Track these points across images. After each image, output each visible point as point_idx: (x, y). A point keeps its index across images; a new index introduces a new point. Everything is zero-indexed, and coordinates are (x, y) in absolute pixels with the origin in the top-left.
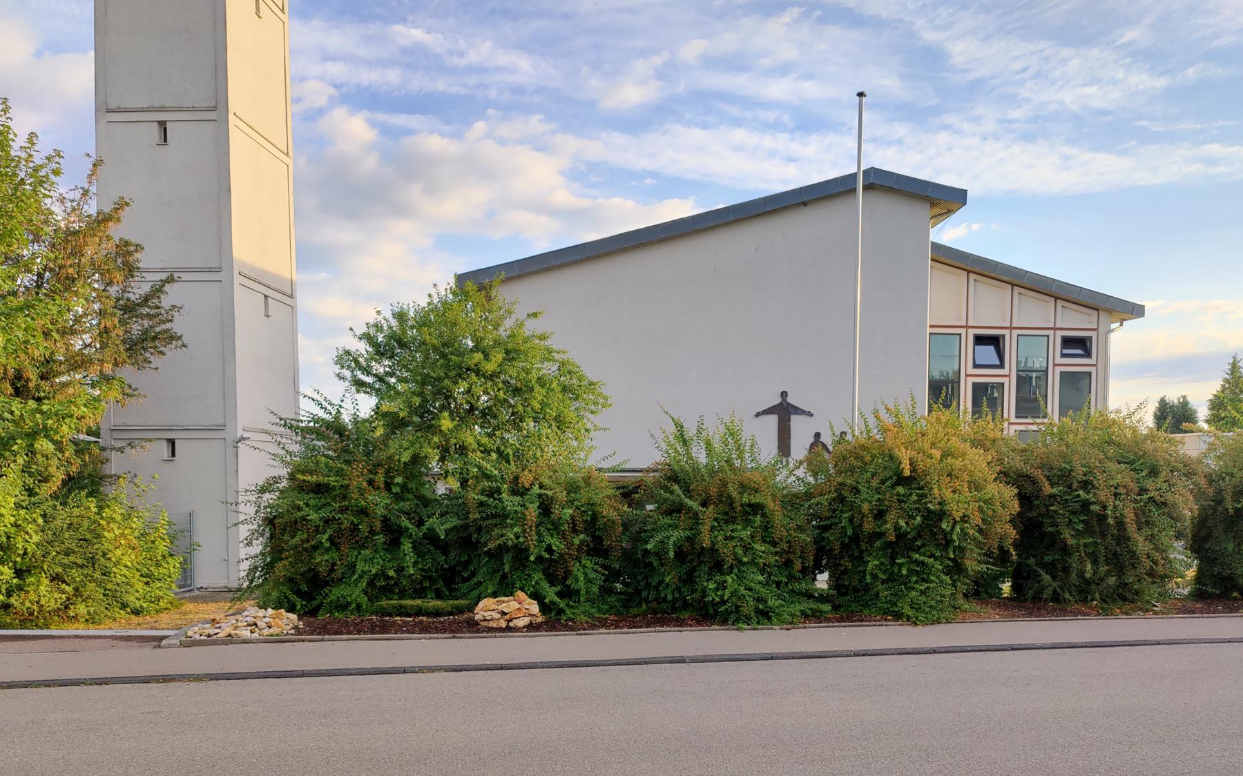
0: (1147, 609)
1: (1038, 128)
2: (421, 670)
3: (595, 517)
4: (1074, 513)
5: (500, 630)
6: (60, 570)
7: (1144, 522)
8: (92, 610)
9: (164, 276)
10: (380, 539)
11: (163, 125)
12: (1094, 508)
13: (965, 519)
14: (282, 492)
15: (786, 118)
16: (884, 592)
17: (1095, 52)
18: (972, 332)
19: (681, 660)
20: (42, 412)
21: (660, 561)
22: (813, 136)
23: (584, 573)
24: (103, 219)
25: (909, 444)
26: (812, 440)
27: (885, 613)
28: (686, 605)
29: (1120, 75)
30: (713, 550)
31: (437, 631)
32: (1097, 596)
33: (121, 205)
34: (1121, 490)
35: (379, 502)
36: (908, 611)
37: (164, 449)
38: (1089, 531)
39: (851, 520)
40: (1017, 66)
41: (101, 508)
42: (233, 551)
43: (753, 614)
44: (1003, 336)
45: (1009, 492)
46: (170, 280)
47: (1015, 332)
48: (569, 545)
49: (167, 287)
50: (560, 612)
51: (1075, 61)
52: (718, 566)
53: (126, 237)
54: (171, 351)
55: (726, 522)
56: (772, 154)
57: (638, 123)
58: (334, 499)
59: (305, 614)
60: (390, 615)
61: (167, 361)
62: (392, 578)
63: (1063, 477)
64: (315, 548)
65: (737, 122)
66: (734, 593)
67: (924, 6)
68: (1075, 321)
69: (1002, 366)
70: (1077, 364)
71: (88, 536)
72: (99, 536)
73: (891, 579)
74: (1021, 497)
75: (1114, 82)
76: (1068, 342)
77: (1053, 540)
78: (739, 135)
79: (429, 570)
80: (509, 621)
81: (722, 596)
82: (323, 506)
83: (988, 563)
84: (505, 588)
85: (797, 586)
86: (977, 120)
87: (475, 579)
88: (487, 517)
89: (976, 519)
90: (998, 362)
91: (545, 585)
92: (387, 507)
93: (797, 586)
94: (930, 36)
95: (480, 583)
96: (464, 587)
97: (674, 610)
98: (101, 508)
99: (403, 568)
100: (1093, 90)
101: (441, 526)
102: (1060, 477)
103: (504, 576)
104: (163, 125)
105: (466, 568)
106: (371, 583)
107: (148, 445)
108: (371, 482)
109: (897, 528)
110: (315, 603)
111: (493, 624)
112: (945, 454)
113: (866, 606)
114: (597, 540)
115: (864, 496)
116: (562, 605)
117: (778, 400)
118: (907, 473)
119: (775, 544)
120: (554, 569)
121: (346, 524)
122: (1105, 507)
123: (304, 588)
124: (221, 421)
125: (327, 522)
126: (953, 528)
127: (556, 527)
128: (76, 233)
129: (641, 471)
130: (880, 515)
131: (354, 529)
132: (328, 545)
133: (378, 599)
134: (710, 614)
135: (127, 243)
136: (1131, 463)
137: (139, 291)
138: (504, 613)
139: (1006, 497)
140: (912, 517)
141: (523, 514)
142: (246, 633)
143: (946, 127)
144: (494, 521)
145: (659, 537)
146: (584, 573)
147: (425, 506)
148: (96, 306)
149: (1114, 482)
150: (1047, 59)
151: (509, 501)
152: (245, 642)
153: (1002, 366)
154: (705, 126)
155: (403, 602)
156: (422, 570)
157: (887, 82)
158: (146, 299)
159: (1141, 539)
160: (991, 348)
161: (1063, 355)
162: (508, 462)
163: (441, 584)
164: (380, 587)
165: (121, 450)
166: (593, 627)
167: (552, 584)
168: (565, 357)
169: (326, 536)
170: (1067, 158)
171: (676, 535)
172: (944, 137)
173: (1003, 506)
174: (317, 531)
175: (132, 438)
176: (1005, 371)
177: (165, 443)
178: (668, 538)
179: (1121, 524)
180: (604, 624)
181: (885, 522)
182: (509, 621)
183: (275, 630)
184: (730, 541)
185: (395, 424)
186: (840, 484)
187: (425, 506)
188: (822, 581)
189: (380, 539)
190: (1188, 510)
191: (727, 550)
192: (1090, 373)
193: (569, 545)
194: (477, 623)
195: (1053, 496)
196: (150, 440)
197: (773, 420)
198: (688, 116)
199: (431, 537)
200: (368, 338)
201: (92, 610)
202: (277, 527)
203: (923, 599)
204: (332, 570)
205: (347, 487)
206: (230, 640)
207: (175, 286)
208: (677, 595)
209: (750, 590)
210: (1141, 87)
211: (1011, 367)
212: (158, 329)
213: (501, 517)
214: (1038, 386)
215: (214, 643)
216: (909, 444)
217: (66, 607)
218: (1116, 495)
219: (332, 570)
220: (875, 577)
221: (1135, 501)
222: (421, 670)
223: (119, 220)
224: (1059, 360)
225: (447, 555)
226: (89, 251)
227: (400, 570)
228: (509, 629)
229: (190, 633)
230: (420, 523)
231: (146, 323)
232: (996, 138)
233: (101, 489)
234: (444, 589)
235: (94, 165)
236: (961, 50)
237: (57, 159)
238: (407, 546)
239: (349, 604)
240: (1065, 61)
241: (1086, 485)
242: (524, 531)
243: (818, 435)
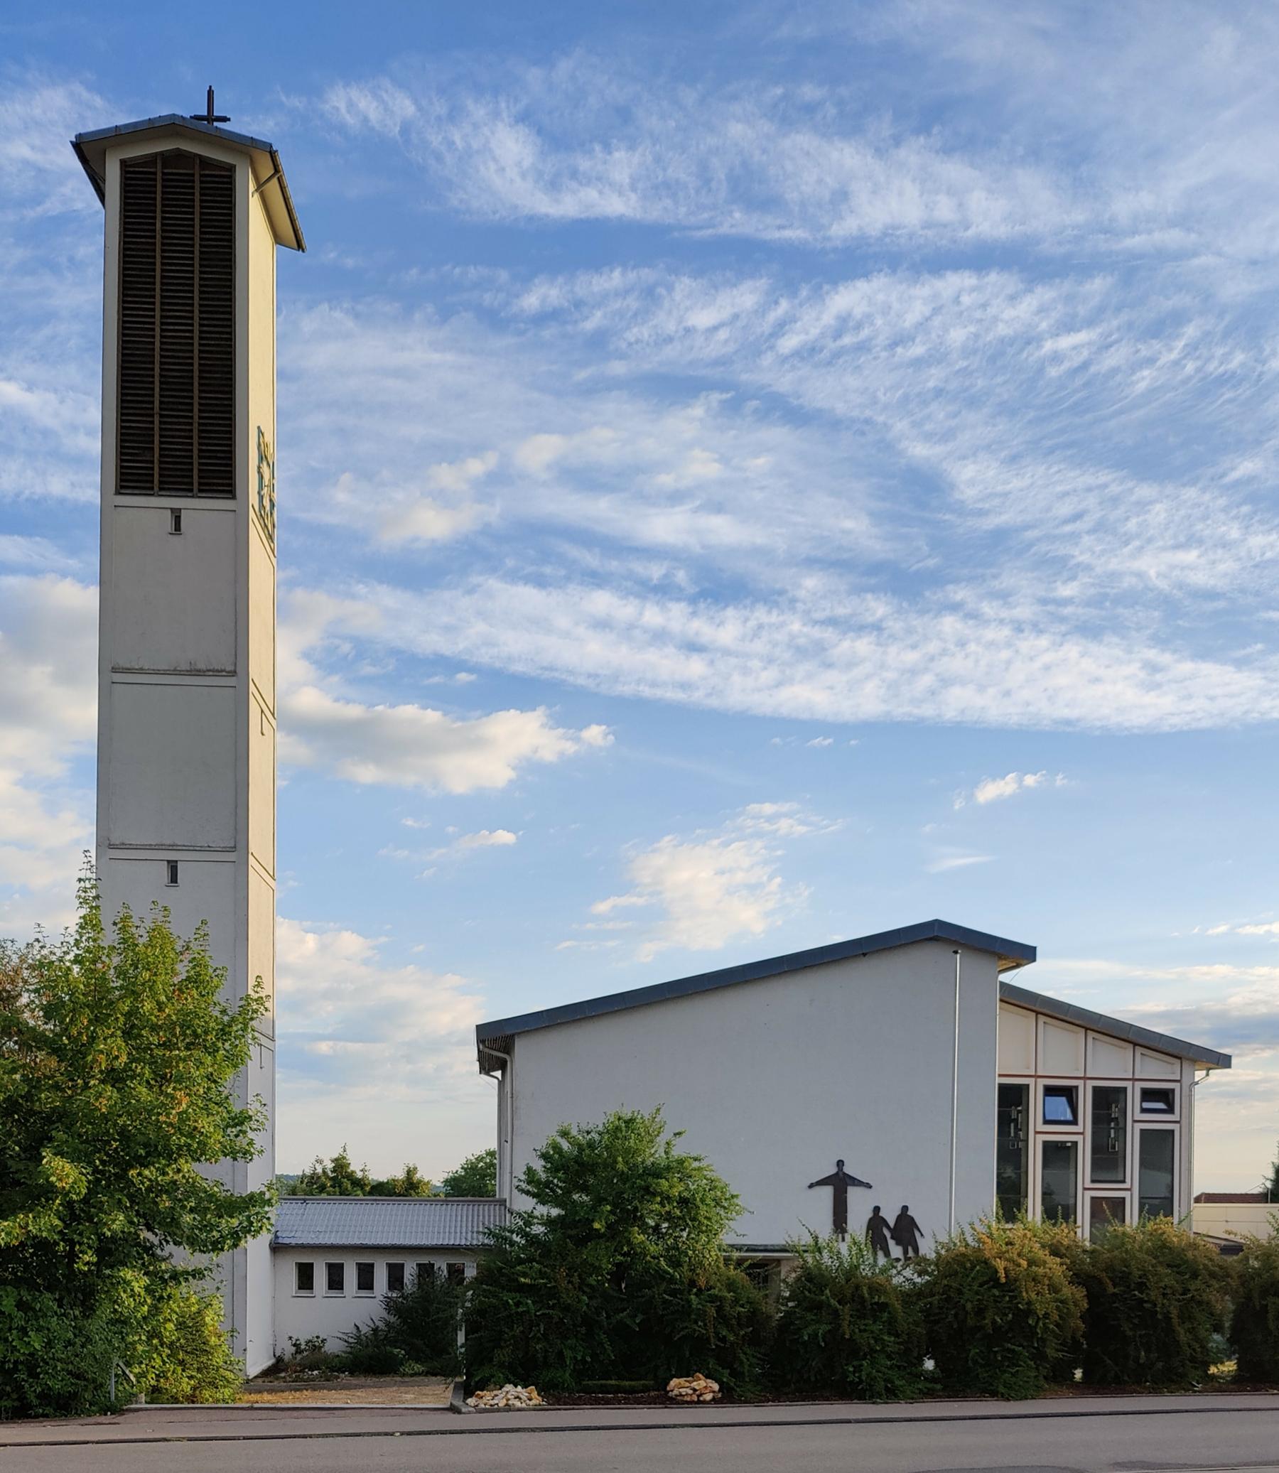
0: (1188, 1389)
1: (1106, 616)
5: (692, 1402)
7: (1186, 1316)
11: (173, 867)
12: (1147, 1305)
13: (1046, 1316)
15: (681, 576)
17: (1190, 493)
19: (849, 1422)
22: (730, 612)
25: (1000, 1255)
26: (871, 1215)
29: (1235, 533)
32: (1149, 1377)
34: (1168, 1291)
39: (956, 1315)
40: (1065, 509)
45: (1080, 1293)
51: (1158, 507)
56: (659, 637)
57: (419, 572)
63: (1122, 1278)
65: (597, 579)
67: (906, 399)
68: (1156, 1071)
69: (1074, 1122)
74: (1089, 1296)
75: (1225, 544)
76: (1148, 1095)
78: (602, 601)
80: (699, 1396)
81: (859, 1377)
86: (1004, 597)
89: (1055, 1316)
90: (1069, 1117)
94: (919, 451)
100: (1191, 556)
102: (1121, 1278)
104: (173, 867)
112: (1031, 1263)
115: (966, 1297)
117: (833, 1170)
118: (1003, 1280)
119: (897, 1336)
121: (556, 1319)
122: (1155, 1305)
126: (1037, 1323)
130: (980, 1312)
136: (1178, 1266)
138: (695, 1390)
140: (1007, 1315)
143: (955, 608)
145: (810, 1330)
149: (1162, 1284)
150: (1115, 500)
152: (519, 1410)
153: (1074, 1122)
154: (540, 582)
157: (849, 524)
159: (1182, 1331)
161: (1144, 1111)
170: (1153, 668)
172: (950, 624)
173: (1076, 1305)
179: (1167, 1317)
181: (984, 1318)
190: (1225, 1305)
192: (1173, 1131)
195: (1114, 1294)
197: (827, 1192)
198: (510, 563)
200: (545, 1156)
203: (1014, 1379)
210: (1269, 555)
214: (1116, 1139)
215: (499, 1410)
216: (1000, 1255)
218: (1164, 1294)
221: (1179, 1300)
228: (699, 1402)
232: (1038, 629)
236: (972, 478)
240: (1143, 506)
241: (1142, 1286)
243: (877, 1209)
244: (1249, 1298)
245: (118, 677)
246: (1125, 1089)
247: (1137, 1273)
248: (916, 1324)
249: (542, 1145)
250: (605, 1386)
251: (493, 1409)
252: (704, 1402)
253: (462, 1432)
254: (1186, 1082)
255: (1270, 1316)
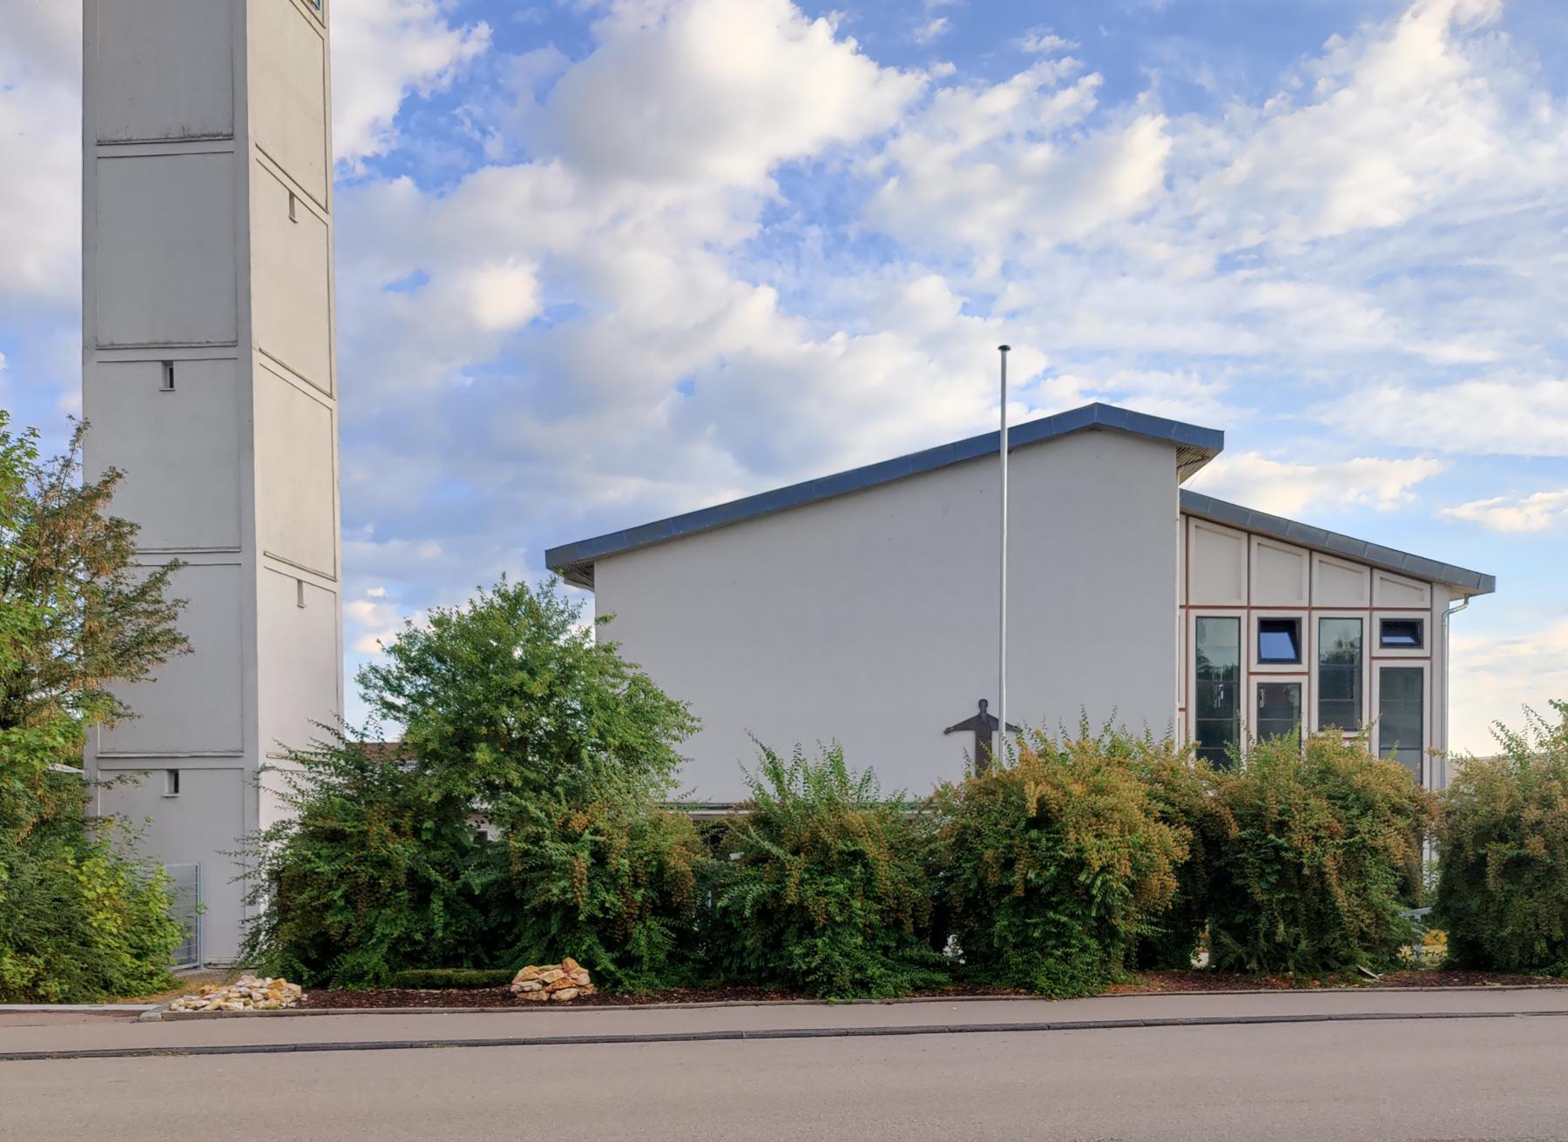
2: (430, 1045)
3: (662, 867)
4: (1265, 861)
5: (540, 1003)
6: (27, 937)
8: (66, 987)
9: (166, 560)
10: (404, 895)
11: (168, 365)
12: (1290, 855)
14: (292, 840)
16: (1015, 958)
18: (1255, 615)
20: (9, 743)
21: (753, 924)
23: (648, 936)
24: (91, 496)
27: (1018, 985)
28: (773, 976)
30: (801, 907)
31: (465, 1003)
32: (1291, 964)
33: (113, 476)
34: (1322, 833)
35: (403, 852)
36: (1042, 982)
37: (165, 781)
38: (1283, 883)
41: (80, 860)
42: (231, 910)
43: (848, 985)
44: (1299, 620)
46: (174, 566)
47: (1316, 615)
48: (629, 902)
49: (170, 577)
50: (618, 983)
52: (808, 928)
53: (118, 516)
54: (173, 657)
55: (822, 874)
58: (351, 848)
59: (315, 986)
60: (414, 987)
61: (169, 670)
62: (419, 942)
63: (1253, 816)
64: (327, 907)
66: (825, 960)
68: (1400, 599)
69: (1298, 660)
70: (1402, 657)
71: (65, 896)
72: (77, 896)
73: (1024, 943)
76: (1389, 627)
77: (1241, 897)
79: (465, 933)
82: (337, 857)
83: (1151, 923)
84: (552, 955)
85: (908, 952)
87: (519, 945)
88: (532, 869)
89: (1124, 868)
90: (1291, 654)
91: (600, 951)
92: (413, 858)
93: (908, 952)
95: (525, 949)
96: (506, 955)
97: (760, 982)
98: (80, 860)
99: (433, 931)
101: (477, 881)
103: (553, 941)
104: (168, 365)
105: (509, 932)
106: (393, 949)
107: (142, 778)
108: (396, 828)
109: (1027, 882)
110: (326, 973)
111: (531, 996)
113: (998, 976)
114: (664, 896)
116: (619, 975)
117: (975, 712)
119: (879, 900)
120: (611, 931)
121: (363, 878)
123: (313, 955)
124: (238, 746)
125: (342, 875)
127: (613, 880)
128: (55, 514)
129: (727, 807)
130: (1008, 865)
131: (373, 883)
132: (342, 903)
133: (402, 968)
134: (797, 986)
135: (119, 523)
136: (1344, 798)
137: (134, 582)
138: (545, 984)
139: (1173, 843)
141: (571, 864)
142: (238, 1005)
144: (542, 873)
145: (736, 891)
146: (648, 936)
147: (463, 856)
148: (80, 603)
151: (555, 850)
152: (237, 1015)
153: (1298, 660)
155: (432, 972)
156: (456, 933)
158: (143, 592)
160: (1285, 636)
161: (1384, 645)
162: (559, 802)
163: (479, 951)
164: (405, 953)
165: (108, 785)
166: (654, 1000)
167: (609, 949)
168: (638, 672)
169: (339, 893)
171: (756, 890)
174: (330, 887)
175: (127, 768)
176: (1303, 668)
177: (166, 774)
178: (747, 892)
180: (667, 997)
182: (552, 992)
183: (272, 1002)
184: (822, 897)
185: (428, 757)
186: (964, 827)
187: (463, 856)
188: (951, 948)
189: (404, 895)
191: (819, 908)
193: (629, 902)
194: (513, 996)
195: (1243, 841)
196: (146, 772)
197: (968, 738)
199: (466, 891)
200: (397, 650)
201: (66, 987)
202: (287, 881)
204: (346, 934)
205: (365, 833)
206: (219, 1013)
207: (181, 572)
208: (762, 963)
209: (847, 955)
211: (1311, 662)
212: (157, 630)
213: (546, 868)
215: (201, 1016)
217: (36, 985)
219: (346, 934)
220: (1004, 939)
222: (430, 1045)
223: (109, 495)
224: (1378, 652)
225: (486, 915)
226: (71, 536)
227: (429, 933)
228: (551, 1002)
229: (174, 1006)
230: (455, 876)
231: (143, 622)
233: (82, 836)
234: (484, 956)
235: (79, 430)
237: (32, 439)
238: (437, 904)
239: (366, 973)
241: (1281, 827)
242: (573, 886)
244: (1458, 846)
245: (104, 151)
246: (1421, 670)
247: (1275, 808)
248: (913, 882)
249: (391, 640)
250: (428, 977)
251: (197, 1014)
252: (559, 1002)
253: (119, 1054)
254: (1437, 611)
255: (1491, 871)
